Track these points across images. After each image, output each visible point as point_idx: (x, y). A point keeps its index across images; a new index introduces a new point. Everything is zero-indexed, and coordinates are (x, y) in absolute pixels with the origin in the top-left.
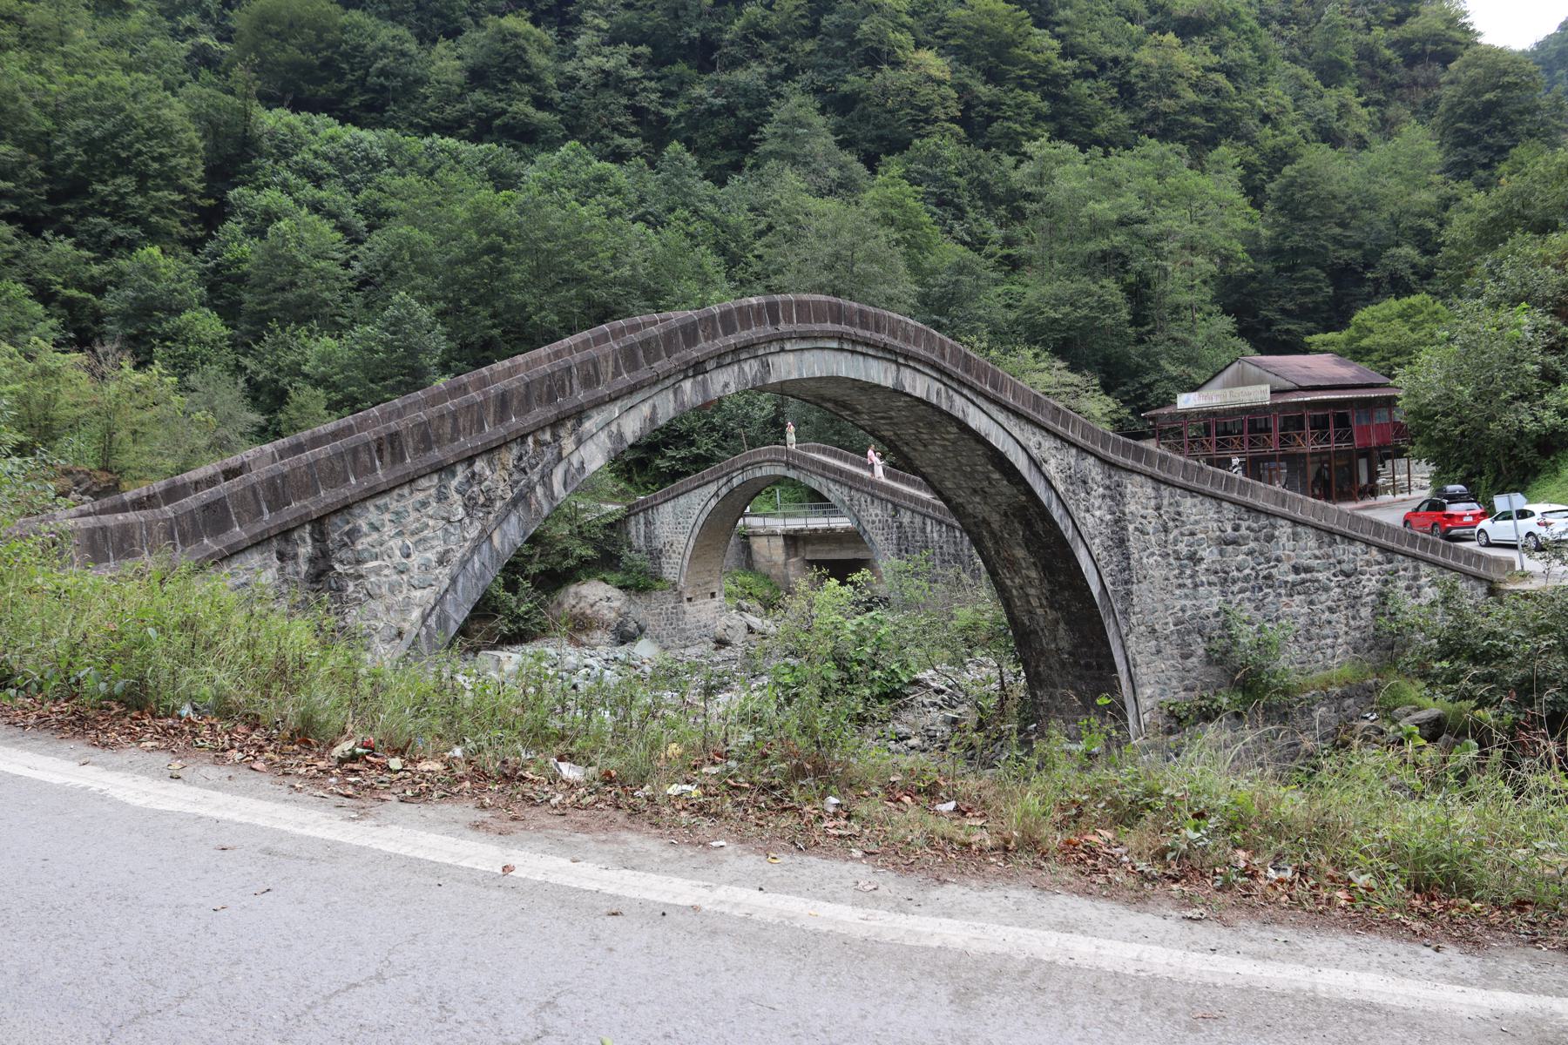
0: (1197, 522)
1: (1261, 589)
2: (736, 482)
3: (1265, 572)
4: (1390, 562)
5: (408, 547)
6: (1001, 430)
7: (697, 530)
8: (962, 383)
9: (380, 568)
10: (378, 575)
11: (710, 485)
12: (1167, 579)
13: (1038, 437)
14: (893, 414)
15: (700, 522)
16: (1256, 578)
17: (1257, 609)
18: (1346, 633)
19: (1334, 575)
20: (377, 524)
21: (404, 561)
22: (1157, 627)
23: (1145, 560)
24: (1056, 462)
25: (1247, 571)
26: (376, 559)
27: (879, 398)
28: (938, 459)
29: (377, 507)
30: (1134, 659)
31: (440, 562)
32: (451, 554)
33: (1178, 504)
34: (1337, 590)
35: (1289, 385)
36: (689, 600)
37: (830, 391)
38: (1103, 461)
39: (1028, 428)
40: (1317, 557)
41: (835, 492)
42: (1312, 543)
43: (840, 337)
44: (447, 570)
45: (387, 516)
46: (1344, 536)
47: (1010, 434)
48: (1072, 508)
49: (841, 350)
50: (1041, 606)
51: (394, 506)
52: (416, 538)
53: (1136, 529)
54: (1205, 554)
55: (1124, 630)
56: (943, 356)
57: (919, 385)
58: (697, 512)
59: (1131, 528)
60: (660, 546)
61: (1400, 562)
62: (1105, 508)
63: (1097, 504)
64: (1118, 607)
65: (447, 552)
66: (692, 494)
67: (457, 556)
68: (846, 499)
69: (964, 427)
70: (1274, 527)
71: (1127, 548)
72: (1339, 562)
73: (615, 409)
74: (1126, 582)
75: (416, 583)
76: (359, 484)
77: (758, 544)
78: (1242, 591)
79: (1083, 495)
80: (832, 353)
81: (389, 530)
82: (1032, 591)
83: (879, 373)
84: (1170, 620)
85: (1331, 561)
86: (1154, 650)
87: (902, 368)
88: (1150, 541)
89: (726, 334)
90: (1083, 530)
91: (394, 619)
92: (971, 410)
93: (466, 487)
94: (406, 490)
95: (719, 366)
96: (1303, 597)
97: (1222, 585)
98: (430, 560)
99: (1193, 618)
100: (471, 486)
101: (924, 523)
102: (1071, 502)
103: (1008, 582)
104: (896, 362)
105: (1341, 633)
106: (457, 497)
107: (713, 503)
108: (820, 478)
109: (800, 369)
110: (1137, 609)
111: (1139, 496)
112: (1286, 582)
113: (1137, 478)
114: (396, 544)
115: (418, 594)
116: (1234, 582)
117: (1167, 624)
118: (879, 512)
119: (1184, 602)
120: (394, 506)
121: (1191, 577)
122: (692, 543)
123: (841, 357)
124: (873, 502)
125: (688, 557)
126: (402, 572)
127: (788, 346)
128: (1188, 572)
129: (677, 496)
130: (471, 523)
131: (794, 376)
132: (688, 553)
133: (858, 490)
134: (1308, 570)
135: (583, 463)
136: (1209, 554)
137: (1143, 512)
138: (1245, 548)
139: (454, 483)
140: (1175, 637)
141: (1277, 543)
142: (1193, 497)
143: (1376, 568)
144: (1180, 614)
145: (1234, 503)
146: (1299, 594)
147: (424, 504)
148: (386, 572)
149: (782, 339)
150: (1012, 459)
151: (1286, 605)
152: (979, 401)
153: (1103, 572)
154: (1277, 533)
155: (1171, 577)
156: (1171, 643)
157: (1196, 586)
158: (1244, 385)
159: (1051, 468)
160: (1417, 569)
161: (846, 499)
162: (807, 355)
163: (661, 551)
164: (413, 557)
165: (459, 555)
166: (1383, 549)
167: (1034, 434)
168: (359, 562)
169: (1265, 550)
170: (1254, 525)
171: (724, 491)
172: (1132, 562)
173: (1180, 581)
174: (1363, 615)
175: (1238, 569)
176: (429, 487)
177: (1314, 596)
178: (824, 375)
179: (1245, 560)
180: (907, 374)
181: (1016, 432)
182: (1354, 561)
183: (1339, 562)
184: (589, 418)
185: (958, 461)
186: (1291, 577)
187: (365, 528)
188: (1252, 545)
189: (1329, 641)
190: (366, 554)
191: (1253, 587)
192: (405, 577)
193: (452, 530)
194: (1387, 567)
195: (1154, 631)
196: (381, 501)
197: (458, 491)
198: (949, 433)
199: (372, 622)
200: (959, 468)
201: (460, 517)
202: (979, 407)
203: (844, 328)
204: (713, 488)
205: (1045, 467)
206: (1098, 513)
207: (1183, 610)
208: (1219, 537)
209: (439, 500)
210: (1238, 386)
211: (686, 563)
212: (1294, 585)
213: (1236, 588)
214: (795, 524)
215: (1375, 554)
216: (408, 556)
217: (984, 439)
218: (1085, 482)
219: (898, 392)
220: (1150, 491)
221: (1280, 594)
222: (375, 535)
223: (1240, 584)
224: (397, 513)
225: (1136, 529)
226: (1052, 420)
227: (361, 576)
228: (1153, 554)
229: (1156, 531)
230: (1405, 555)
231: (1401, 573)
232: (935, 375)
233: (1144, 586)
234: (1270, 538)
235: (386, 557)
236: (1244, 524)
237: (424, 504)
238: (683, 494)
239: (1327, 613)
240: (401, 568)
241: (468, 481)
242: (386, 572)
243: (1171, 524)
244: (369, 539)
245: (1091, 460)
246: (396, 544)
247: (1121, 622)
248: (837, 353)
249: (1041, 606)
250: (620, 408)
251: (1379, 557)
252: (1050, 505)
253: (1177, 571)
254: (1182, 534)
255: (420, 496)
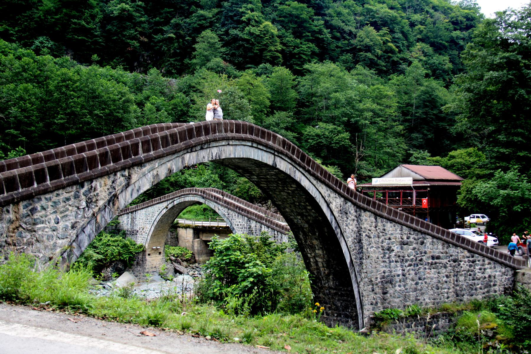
0: (392, 234)
1: (417, 265)
2: (176, 203)
3: (420, 258)
4: (473, 257)
5: (58, 219)
6: (314, 187)
7: (156, 223)
8: (299, 165)
9: (44, 228)
10: (43, 231)
11: (164, 203)
12: (378, 258)
13: (329, 192)
14: (268, 177)
15: (158, 220)
16: (416, 260)
17: (416, 274)
18: (453, 287)
19: (449, 261)
20: (45, 207)
21: (56, 225)
22: (373, 279)
23: (369, 249)
24: (336, 202)
25: (412, 257)
26: (43, 223)
27: (264, 170)
28: (284, 198)
29: (46, 199)
30: (362, 293)
31: (73, 227)
32: (78, 224)
33: (384, 226)
34: (450, 268)
35: (421, 178)
36: (149, 255)
37: (244, 164)
38: (354, 204)
39: (324, 187)
40: (442, 253)
41: (221, 210)
42: (440, 247)
43: (253, 141)
44: (75, 231)
45: (50, 203)
46: (453, 244)
47: (318, 190)
48: (341, 225)
49: (252, 146)
50: (323, 267)
51: (55, 199)
52: (63, 215)
53: (366, 235)
54: (395, 248)
55: (359, 280)
56: (293, 153)
57: (283, 165)
58: (156, 215)
59: (364, 234)
60: (138, 229)
61: (476, 257)
62: (354, 225)
63: (351, 223)
64: (357, 268)
65: (76, 223)
66: (154, 206)
67: (79, 226)
68: (226, 214)
69: (298, 184)
70: (424, 239)
71: (362, 243)
72: (451, 256)
73: (156, 163)
74: (361, 259)
75: (60, 236)
76: (38, 187)
77: (182, 232)
78: (410, 265)
79: (345, 219)
80: (248, 148)
81: (50, 210)
82: (319, 260)
83: (267, 158)
84: (379, 276)
85: (448, 255)
86: (371, 290)
87: (276, 157)
88: (371, 241)
89: (206, 135)
90: (345, 234)
91: (48, 254)
92: (303, 178)
93: (88, 193)
94: (60, 192)
95: (202, 149)
96: (435, 270)
97: (401, 262)
98: (67, 226)
99: (388, 276)
100: (90, 193)
101: (261, 227)
102: (340, 221)
103: (309, 255)
104: (274, 154)
105: (451, 287)
106: (83, 197)
107: (164, 211)
108: (215, 204)
109: (235, 154)
110: (365, 271)
111: (368, 219)
112: (428, 263)
113: (368, 213)
114: (53, 217)
115: (60, 242)
116: (407, 261)
117: (377, 278)
118: (241, 221)
119: (384, 269)
120: (55, 199)
121: (388, 258)
122: (153, 229)
123: (252, 149)
124: (238, 216)
125: (150, 235)
126: (54, 230)
127: (231, 143)
128: (387, 256)
129: (148, 207)
130: (88, 210)
131: (232, 156)
132: (151, 233)
133: (232, 210)
134: (438, 258)
135: (140, 187)
136: (396, 248)
137: (369, 228)
138: (411, 247)
139: (83, 191)
140: (380, 284)
141: (425, 245)
142: (391, 223)
143: (466, 259)
144: (383, 274)
145: (407, 226)
146: (434, 268)
147: (68, 199)
148: (47, 230)
149: (229, 140)
150: (318, 201)
151: (429, 273)
152: (306, 174)
153: (352, 253)
154: (425, 241)
155: (380, 258)
156: (378, 287)
157: (390, 262)
158: (401, 177)
159: (333, 206)
160: (484, 261)
161: (226, 214)
162: (238, 148)
163: (138, 231)
164: (60, 224)
165: (81, 224)
166: (469, 251)
167: (327, 190)
168: (35, 224)
169: (420, 248)
170: (416, 237)
171: (170, 206)
172: (364, 250)
173: (384, 259)
174: (460, 280)
175: (408, 256)
176: (71, 192)
177: (440, 270)
178: (245, 157)
179: (411, 252)
180: (278, 160)
181: (320, 189)
182: (457, 256)
183: (451, 256)
184: (145, 166)
185: (293, 200)
186: (430, 261)
187: (39, 208)
188: (414, 245)
189: (446, 290)
190: (38, 221)
191: (414, 264)
192: (55, 233)
193: (79, 212)
194: (471, 259)
195: (371, 281)
196: (48, 196)
197: (84, 194)
198: (292, 187)
199: (37, 254)
200: (294, 203)
201: (83, 207)
202: (306, 177)
203: (254, 137)
204: (165, 204)
205: (331, 205)
206: (351, 227)
207: (384, 272)
208: (401, 241)
209: (75, 198)
210: (399, 177)
211: (149, 238)
212: (432, 264)
213: (407, 264)
214: (199, 224)
215: (466, 253)
216: (58, 223)
217: (307, 191)
218: (346, 213)
219: (274, 167)
220: (373, 219)
221: (425, 268)
222: (43, 212)
223: (409, 262)
224: (55, 202)
225: (366, 235)
226: (335, 185)
227: (35, 231)
228: (372, 247)
229: (375, 237)
230: (480, 255)
231: (477, 262)
232: (289, 161)
233: (368, 261)
234: (422, 243)
235: (47, 223)
236: (412, 236)
237: (68, 199)
238: (151, 206)
239: (445, 278)
240: (54, 228)
241: (89, 190)
242: (47, 230)
243: (381, 234)
244: (41, 214)
245: (349, 204)
246: (53, 217)
247: (358, 276)
248: (250, 148)
249: (323, 267)
250: (159, 163)
251: (468, 254)
252: (332, 222)
253: (382, 255)
254: (385, 239)
255: (67, 195)
